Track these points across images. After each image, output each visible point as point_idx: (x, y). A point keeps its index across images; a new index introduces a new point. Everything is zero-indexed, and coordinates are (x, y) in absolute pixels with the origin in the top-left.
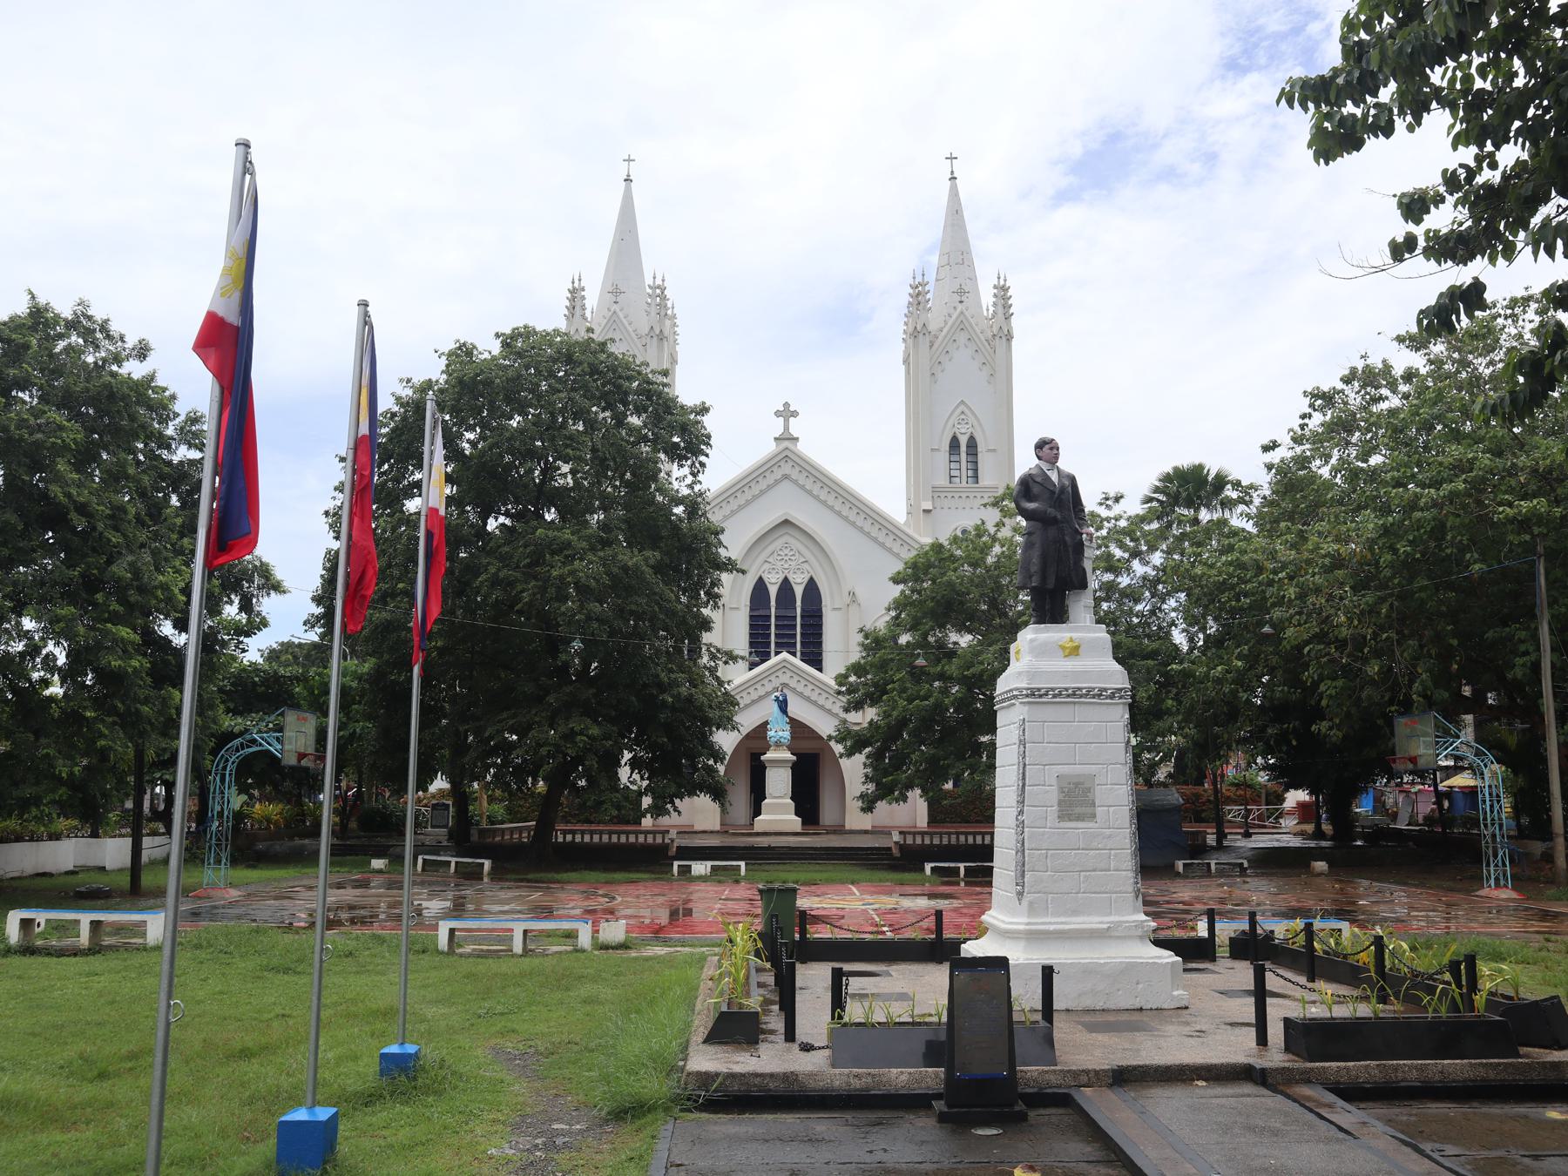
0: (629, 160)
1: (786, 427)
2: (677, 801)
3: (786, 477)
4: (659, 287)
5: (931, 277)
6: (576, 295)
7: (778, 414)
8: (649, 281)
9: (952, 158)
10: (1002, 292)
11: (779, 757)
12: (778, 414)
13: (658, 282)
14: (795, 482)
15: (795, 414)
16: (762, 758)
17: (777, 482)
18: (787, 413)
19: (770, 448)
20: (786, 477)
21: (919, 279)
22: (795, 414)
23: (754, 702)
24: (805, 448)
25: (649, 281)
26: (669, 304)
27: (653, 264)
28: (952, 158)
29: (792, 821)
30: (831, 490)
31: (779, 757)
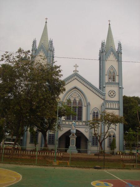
0: (46, 19)
1: (76, 69)
2: (54, 61)
3: (76, 79)
4: (51, 41)
5: (105, 41)
6: (34, 42)
7: (74, 66)
8: (49, 40)
9: (46, 19)
10: (120, 45)
11: (73, 139)
12: (74, 66)
13: (51, 40)
14: (77, 80)
15: (78, 66)
16: (70, 136)
17: (74, 80)
18: (76, 66)
19: (72, 73)
20: (76, 79)
21: (103, 42)
22: (78, 66)
23: (68, 84)
24: (80, 73)
25: (49, 40)
26: (53, 46)
27: (50, 36)
28: (109, 21)
29: (76, 152)
30: (85, 82)
31: (73, 139)
